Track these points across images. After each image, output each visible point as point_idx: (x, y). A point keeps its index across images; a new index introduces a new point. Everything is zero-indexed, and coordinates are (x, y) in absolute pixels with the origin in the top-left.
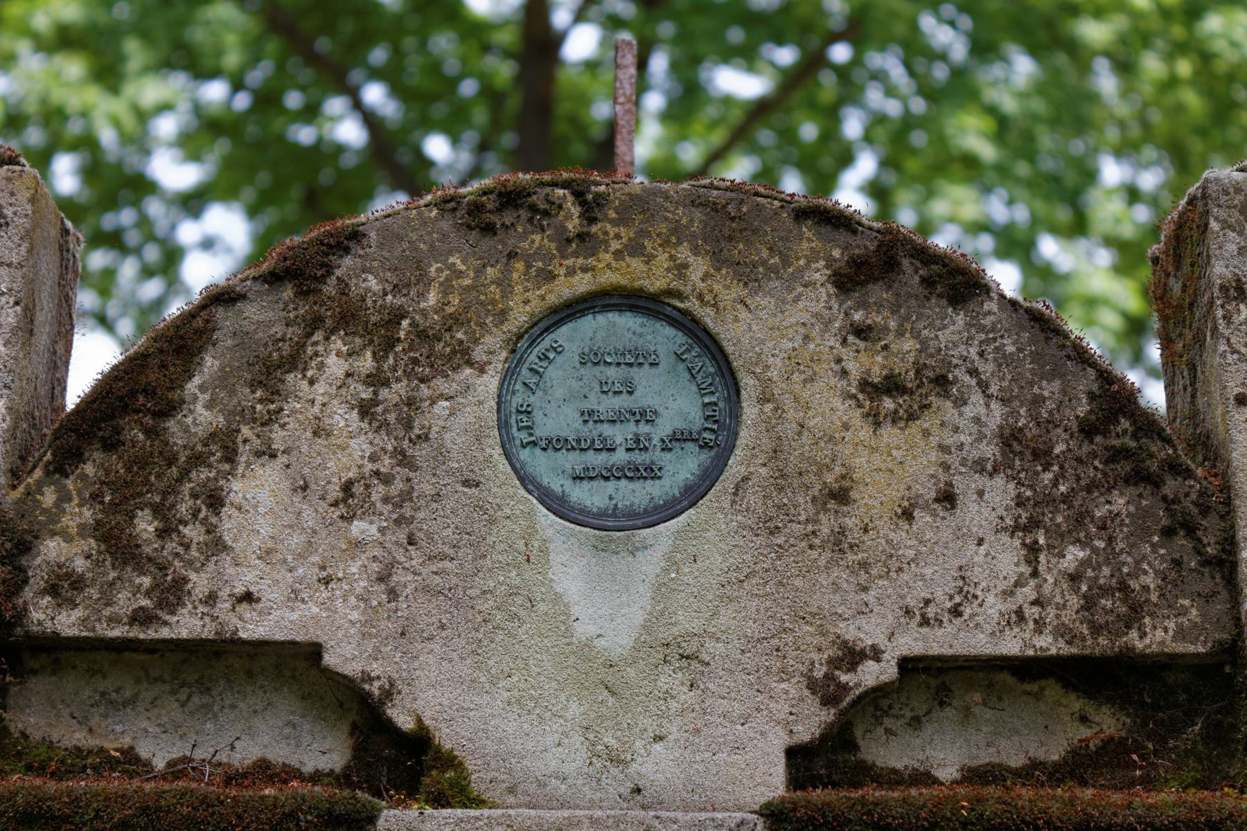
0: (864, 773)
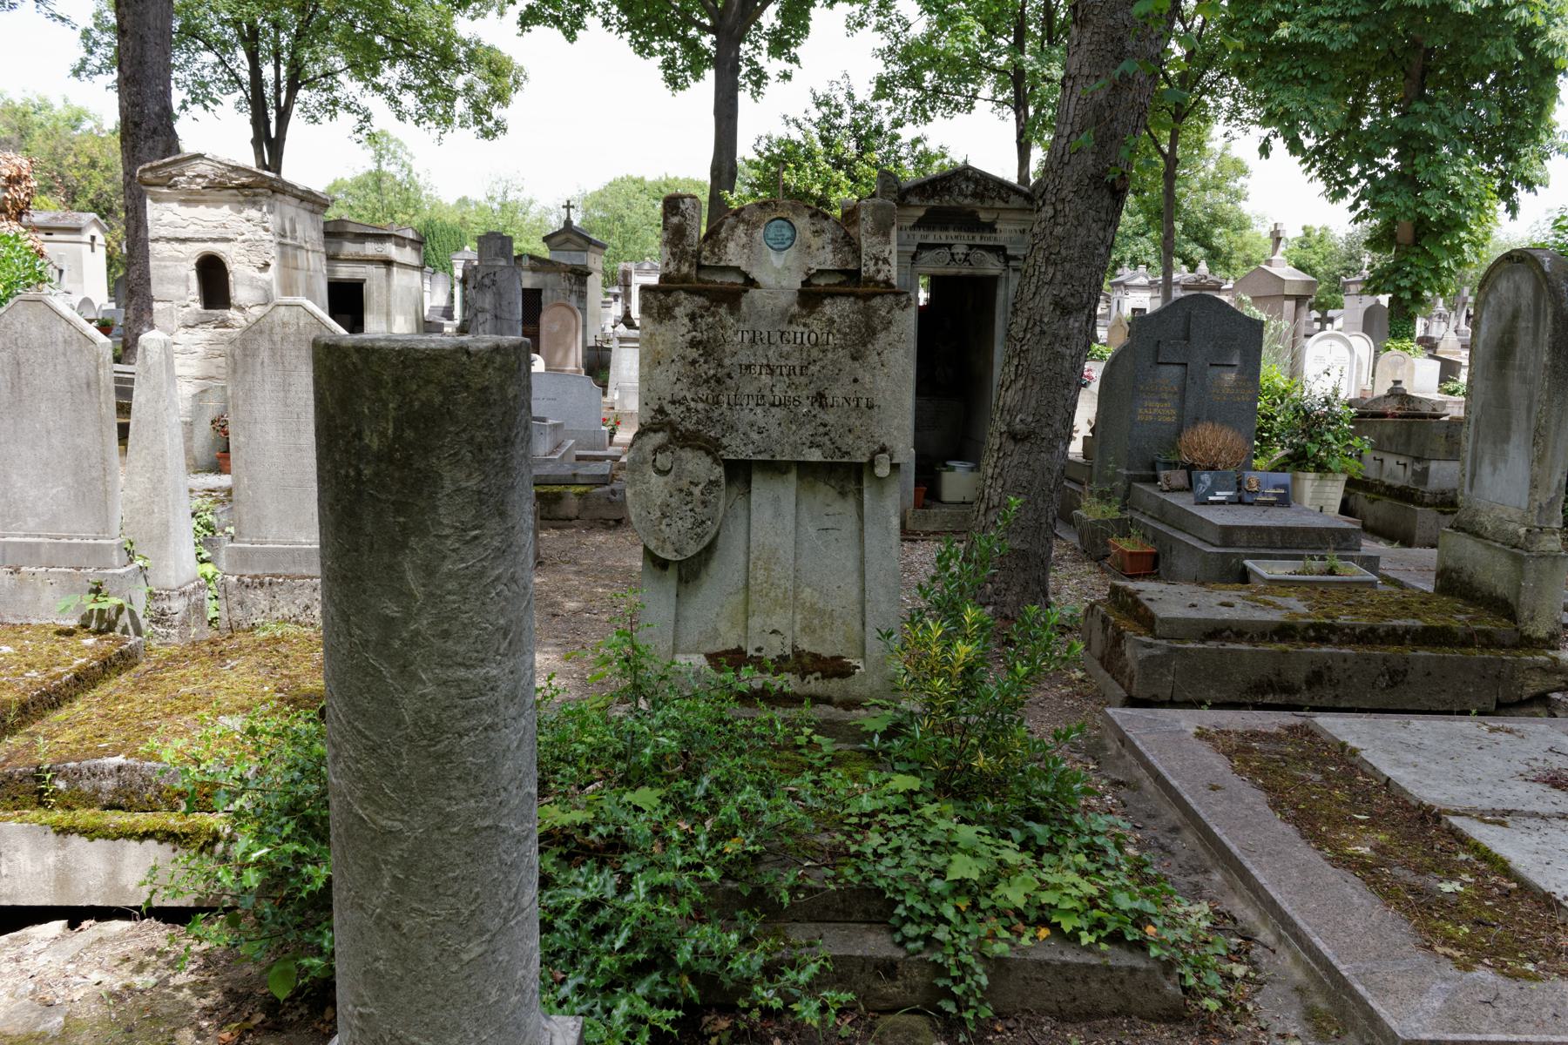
0: (811, 285)
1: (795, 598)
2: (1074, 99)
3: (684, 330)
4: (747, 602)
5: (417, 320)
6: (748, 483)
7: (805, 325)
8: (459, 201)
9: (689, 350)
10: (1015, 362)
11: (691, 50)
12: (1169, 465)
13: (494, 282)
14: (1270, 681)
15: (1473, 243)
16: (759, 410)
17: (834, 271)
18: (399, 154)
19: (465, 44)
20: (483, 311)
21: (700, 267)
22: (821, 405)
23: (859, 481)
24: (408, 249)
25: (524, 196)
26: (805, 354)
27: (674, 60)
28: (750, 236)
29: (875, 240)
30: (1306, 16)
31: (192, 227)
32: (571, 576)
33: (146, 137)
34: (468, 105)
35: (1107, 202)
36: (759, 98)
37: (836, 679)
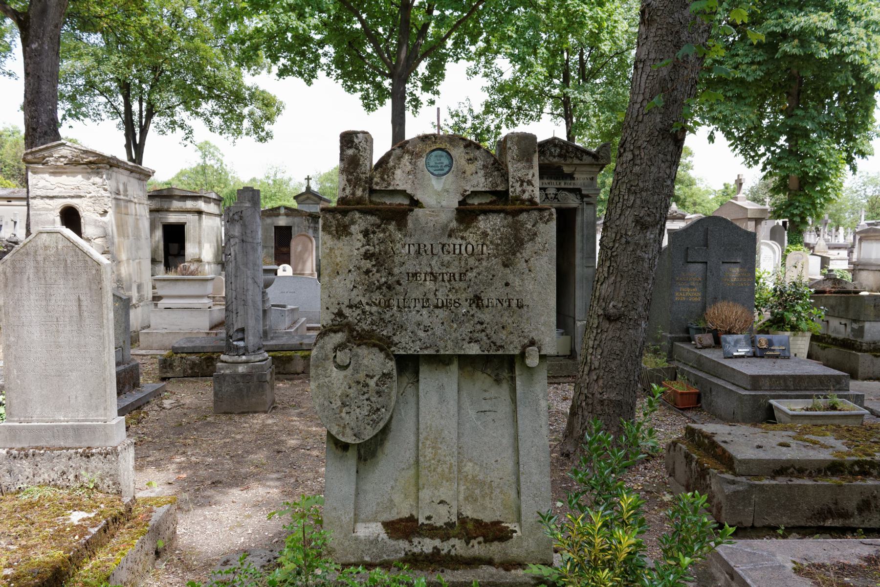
0: (467, 204)
2: (644, 76)
3: (359, 244)
4: (418, 476)
6: (417, 373)
7: (462, 238)
8: (251, 180)
9: (364, 261)
10: (608, 264)
11: (378, 88)
12: (700, 331)
13: (241, 218)
14: (830, 508)
15: (834, 188)
16: (425, 312)
18: (216, 153)
19: (249, 89)
20: (234, 237)
21: (372, 191)
22: (478, 306)
23: (512, 370)
24: (212, 204)
25: (286, 177)
26: (463, 263)
27: (368, 94)
28: (414, 165)
30: (731, 62)
31: (58, 189)
33: (40, 137)
35: (671, 148)
36: (416, 115)
37: (496, 543)
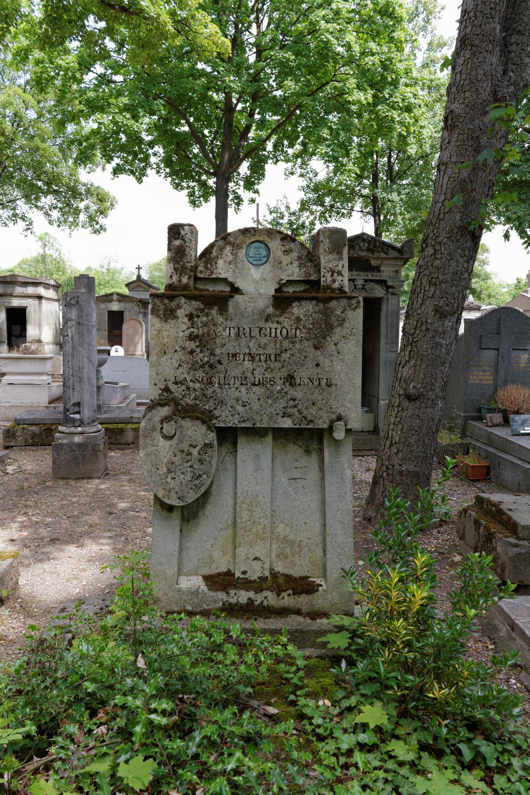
0: (283, 292)
1: (272, 532)
2: (446, 178)
3: (184, 327)
4: (235, 536)
5: (56, 328)
6: (235, 444)
7: (278, 322)
9: (188, 342)
10: (409, 349)
11: (203, 186)
13: (77, 302)
16: (243, 389)
17: (299, 281)
19: (85, 185)
20: (71, 320)
21: (197, 279)
22: (291, 384)
23: (321, 442)
24: (51, 290)
25: (118, 267)
26: (278, 345)
27: (194, 192)
28: (235, 255)
29: (331, 257)
32: (125, 484)
34: (86, 217)
35: (469, 244)
37: (304, 595)
